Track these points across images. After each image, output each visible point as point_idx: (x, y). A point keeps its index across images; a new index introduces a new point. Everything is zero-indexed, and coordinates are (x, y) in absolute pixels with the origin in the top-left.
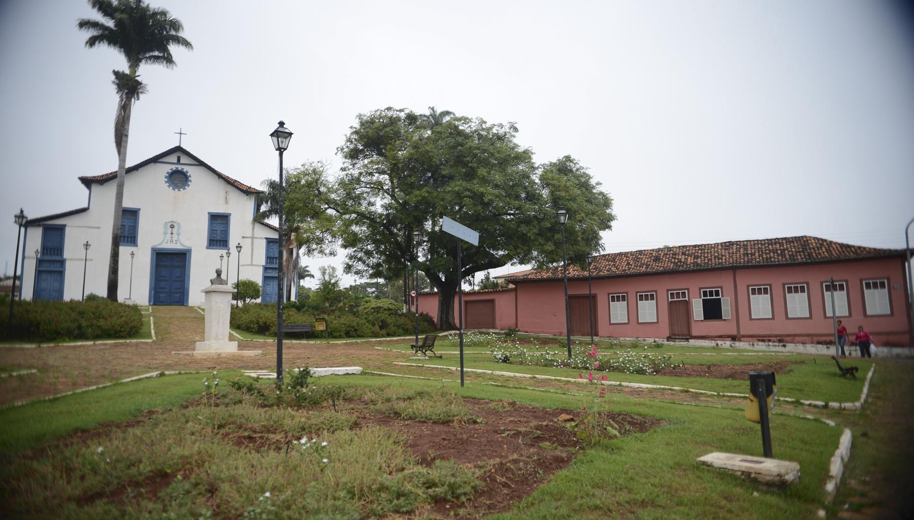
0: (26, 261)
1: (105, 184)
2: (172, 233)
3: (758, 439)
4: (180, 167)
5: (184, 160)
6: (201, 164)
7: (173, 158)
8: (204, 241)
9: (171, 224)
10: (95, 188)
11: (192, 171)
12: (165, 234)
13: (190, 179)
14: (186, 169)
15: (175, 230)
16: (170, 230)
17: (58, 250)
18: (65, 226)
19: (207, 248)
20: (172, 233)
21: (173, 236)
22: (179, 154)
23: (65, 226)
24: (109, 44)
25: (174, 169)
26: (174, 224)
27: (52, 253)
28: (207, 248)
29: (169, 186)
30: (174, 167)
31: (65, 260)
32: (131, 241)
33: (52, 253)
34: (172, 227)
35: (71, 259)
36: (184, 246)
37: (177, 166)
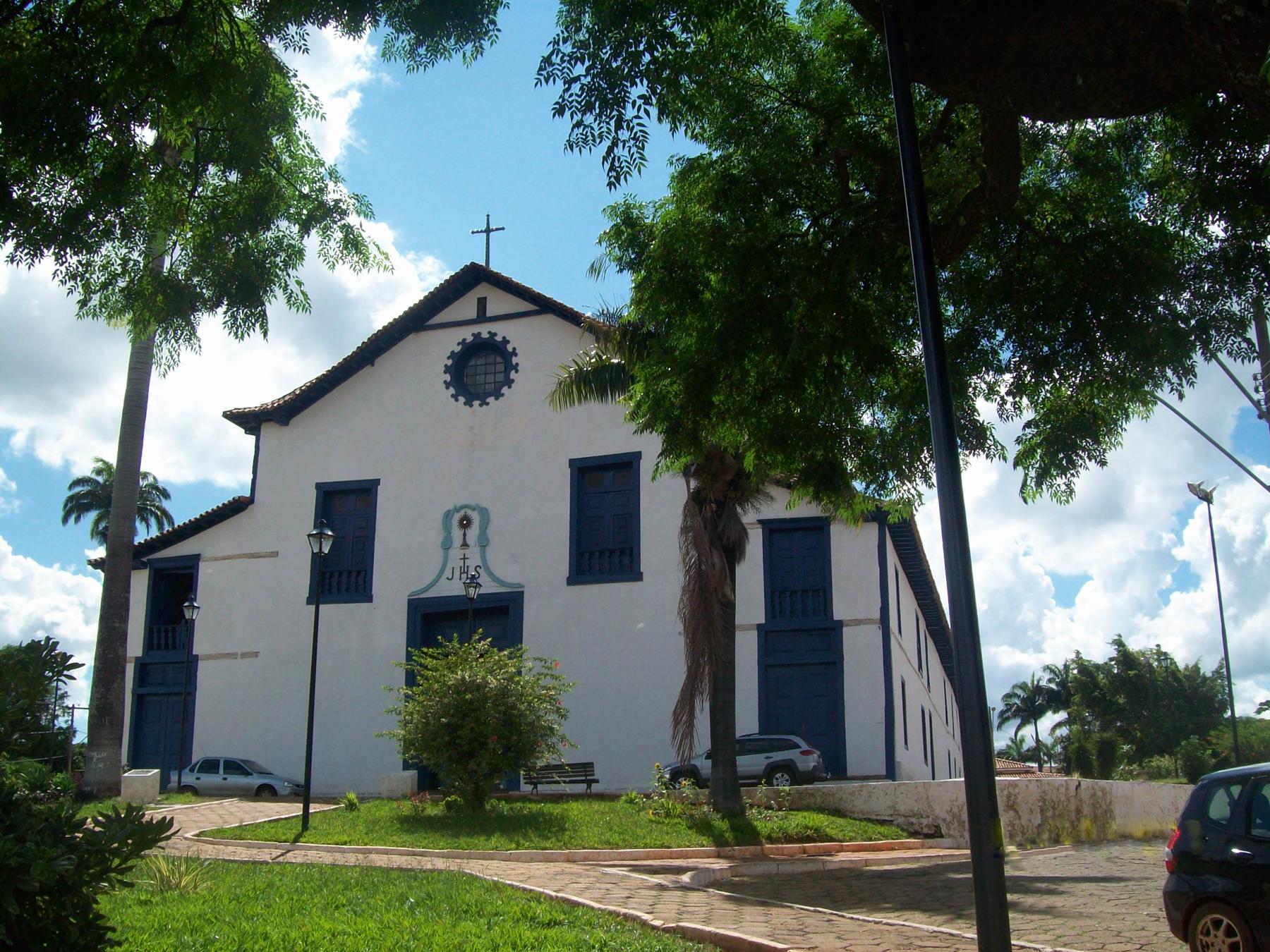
0: (876, 615)
1: (294, 421)
2: (465, 545)
3: (614, 811)
4: (484, 330)
5: (499, 303)
6: (544, 306)
7: (465, 308)
8: (560, 559)
9: (462, 513)
10: (268, 430)
11: (515, 334)
12: (447, 546)
13: (452, 391)
14: (501, 330)
15: (473, 533)
16: (457, 534)
17: (359, 573)
18: (195, 559)
19: (571, 581)
20: (465, 545)
21: (468, 552)
22: (483, 290)
23: (195, 559)
24: (285, 121)
25: (470, 339)
26: (470, 513)
27: (344, 587)
28: (571, 581)
29: (455, 397)
30: (467, 334)
31: (840, 624)
32: (339, 590)
33: (344, 587)
34: (465, 523)
35: (209, 657)
36: (501, 583)
37: (476, 329)
